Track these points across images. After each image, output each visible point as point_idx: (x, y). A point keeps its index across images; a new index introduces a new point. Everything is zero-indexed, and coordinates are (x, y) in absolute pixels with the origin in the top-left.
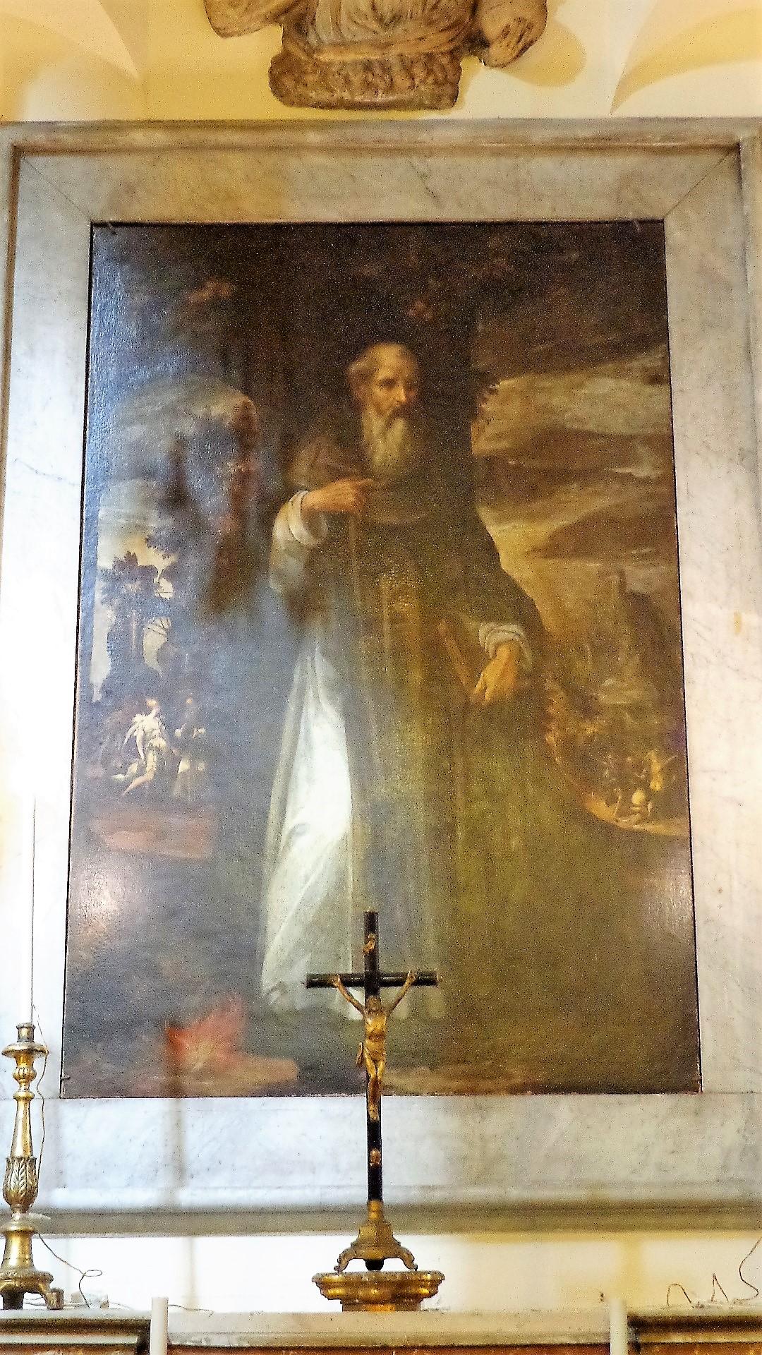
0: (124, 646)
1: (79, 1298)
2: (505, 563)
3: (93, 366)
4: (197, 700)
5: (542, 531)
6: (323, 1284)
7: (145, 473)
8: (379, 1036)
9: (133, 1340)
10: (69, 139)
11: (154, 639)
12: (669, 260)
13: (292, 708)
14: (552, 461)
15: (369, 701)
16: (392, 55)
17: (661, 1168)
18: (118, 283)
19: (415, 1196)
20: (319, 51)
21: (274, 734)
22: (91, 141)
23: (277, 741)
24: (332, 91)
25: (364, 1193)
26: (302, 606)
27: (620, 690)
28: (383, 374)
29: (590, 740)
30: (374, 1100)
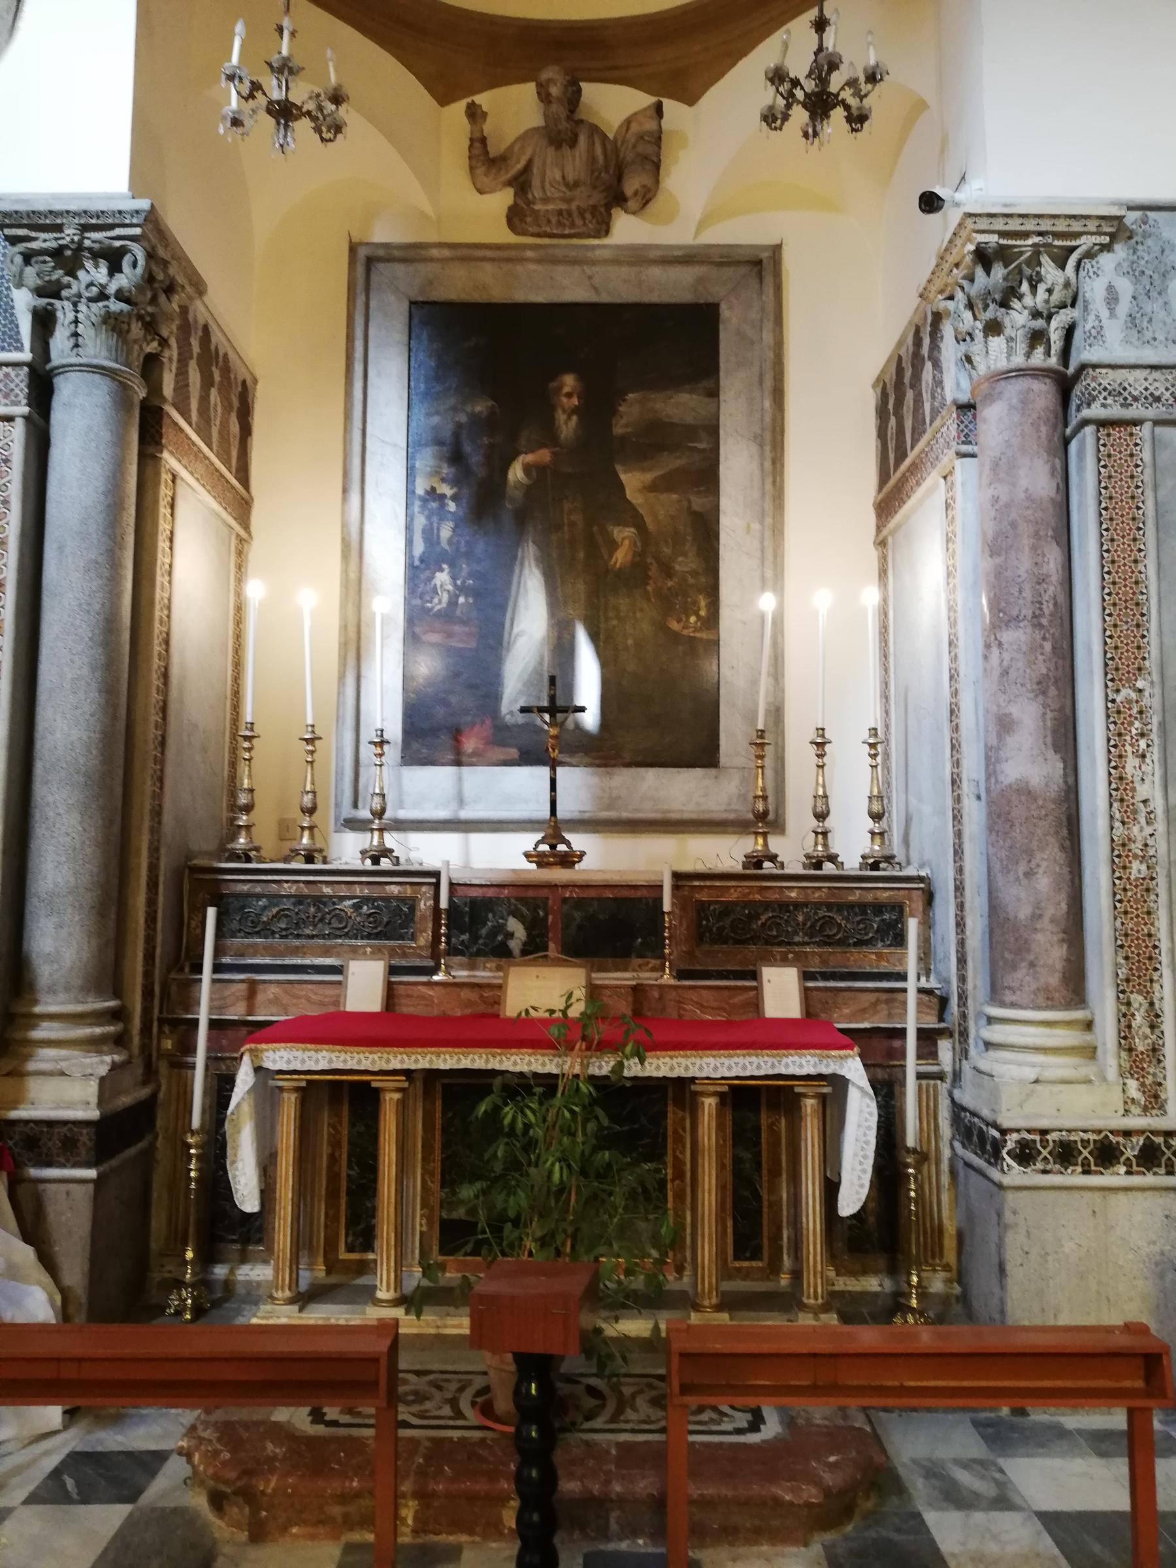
0: (430, 536)
1: (408, 860)
2: (629, 494)
3: (412, 384)
4: (468, 565)
5: (648, 477)
6: (527, 855)
7: (439, 442)
8: (555, 737)
9: (434, 880)
10: (396, 253)
11: (446, 532)
12: (721, 327)
13: (517, 570)
14: (656, 439)
15: (557, 569)
16: (574, 206)
17: (698, 804)
18: (425, 336)
19: (576, 815)
20: (534, 203)
21: (509, 583)
22: (410, 254)
23: (509, 589)
24: (540, 226)
25: (549, 813)
26: (521, 518)
27: (686, 564)
28: (566, 389)
29: (669, 589)
30: (553, 770)
